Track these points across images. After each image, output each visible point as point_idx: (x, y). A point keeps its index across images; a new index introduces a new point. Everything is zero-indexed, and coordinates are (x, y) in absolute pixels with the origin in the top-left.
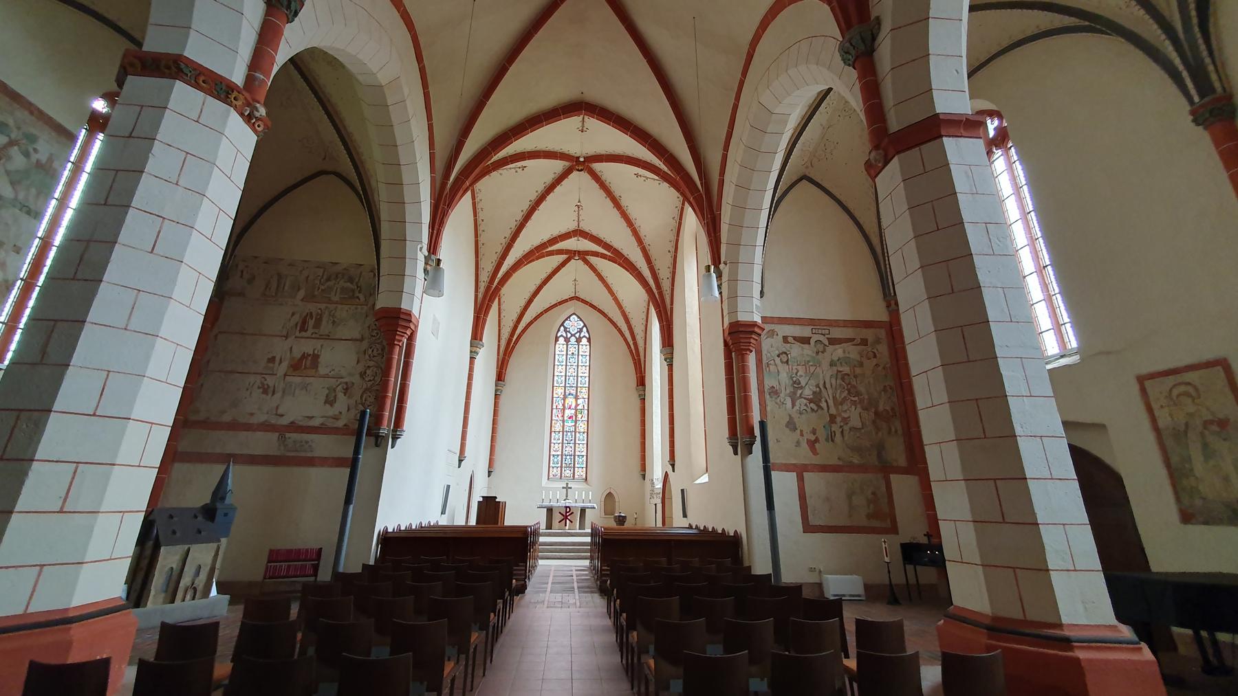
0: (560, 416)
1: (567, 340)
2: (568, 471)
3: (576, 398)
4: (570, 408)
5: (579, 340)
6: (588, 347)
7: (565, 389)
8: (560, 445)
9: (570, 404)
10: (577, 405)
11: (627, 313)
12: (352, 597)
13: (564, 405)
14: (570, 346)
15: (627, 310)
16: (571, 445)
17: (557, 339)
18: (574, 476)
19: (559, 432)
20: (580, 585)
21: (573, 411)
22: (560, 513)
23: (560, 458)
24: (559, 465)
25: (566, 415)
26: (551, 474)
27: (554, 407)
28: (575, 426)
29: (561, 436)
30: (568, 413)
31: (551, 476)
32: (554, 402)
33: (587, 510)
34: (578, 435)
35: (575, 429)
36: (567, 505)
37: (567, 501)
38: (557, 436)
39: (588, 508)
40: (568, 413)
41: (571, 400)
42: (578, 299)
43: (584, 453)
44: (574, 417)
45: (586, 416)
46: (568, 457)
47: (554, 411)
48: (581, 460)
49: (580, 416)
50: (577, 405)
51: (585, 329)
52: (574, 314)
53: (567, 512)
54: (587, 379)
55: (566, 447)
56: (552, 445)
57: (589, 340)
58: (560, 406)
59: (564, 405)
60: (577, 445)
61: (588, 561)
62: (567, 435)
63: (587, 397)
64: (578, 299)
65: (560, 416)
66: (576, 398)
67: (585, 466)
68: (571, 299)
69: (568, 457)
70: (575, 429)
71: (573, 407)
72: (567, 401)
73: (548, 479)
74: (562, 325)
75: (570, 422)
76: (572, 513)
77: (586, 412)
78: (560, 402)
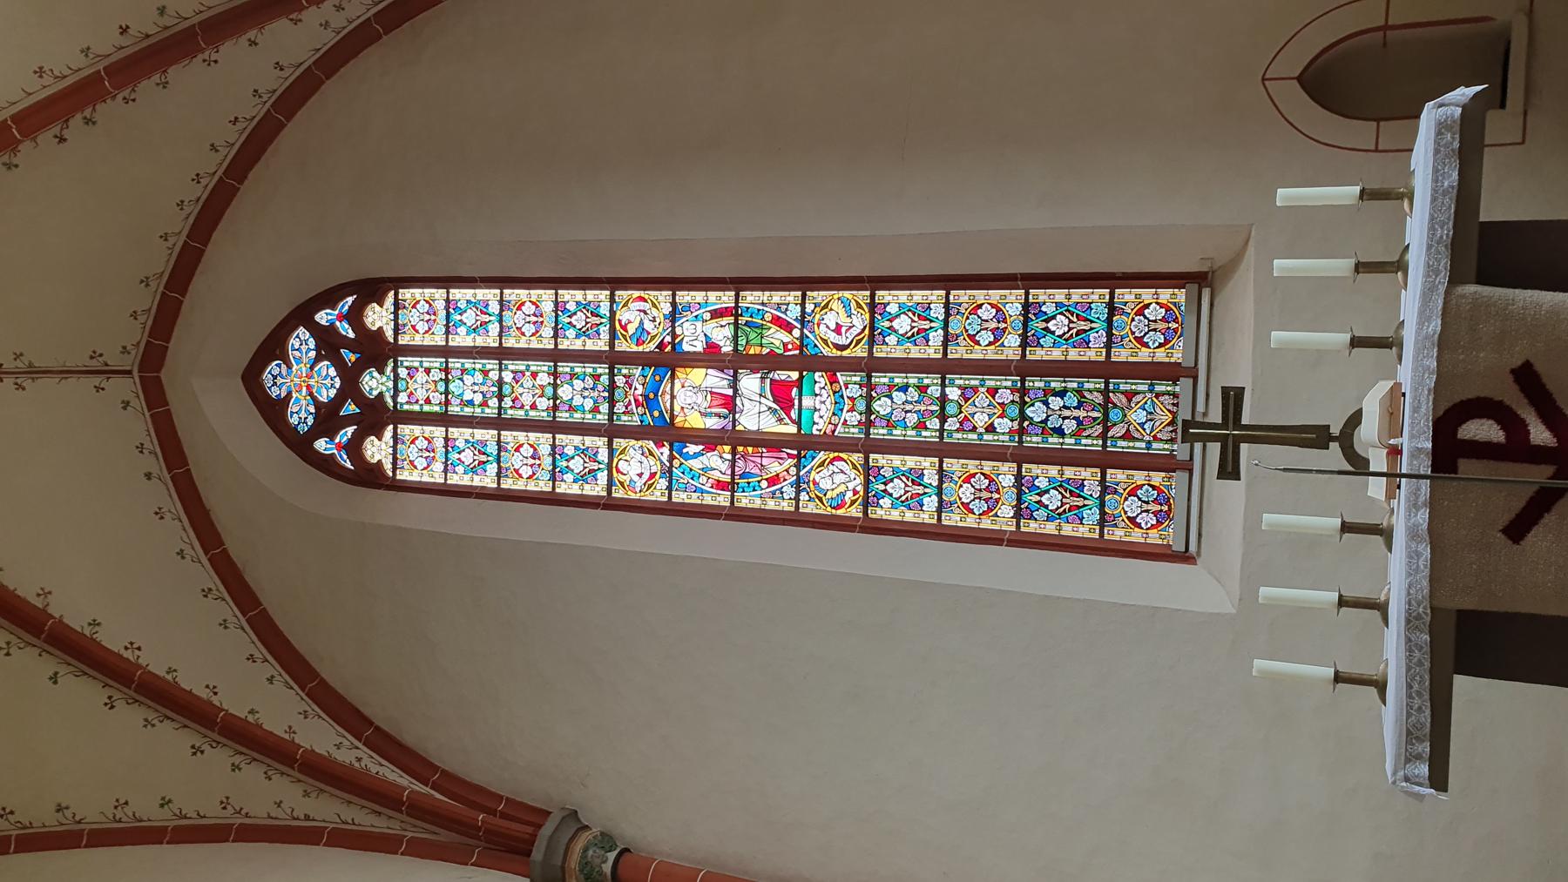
0: (775, 468)
1: (376, 417)
2: (1137, 416)
3: (669, 360)
4: (730, 403)
5: (377, 350)
6: (407, 294)
7: (484, 423)
8: (952, 465)
9: (703, 401)
10: (711, 356)
11: (131, 45)
12: (1275, 275)
13: (709, 441)
14: (403, 398)
15: (108, 44)
16: (953, 393)
17: (371, 477)
18: (1170, 372)
19: (868, 472)
20: (1231, 425)
21: (750, 383)
22: (1517, 530)
23: (1043, 475)
24: (1089, 475)
25: (770, 425)
26: (1154, 538)
27: (723, 499)
28: (833, 368)
29: (896, 460)
30: (756, 415)
31: (1170, 535)
32: (694, 499)
33: (1493, 209)
34: (891, 348)
35: (852, 365)
36: (1416, 440)
37: (1369, 431)
38: (897, 488)
39: (1466, 196)
40: (756, 415)
41: (683, 397)
42: (153, 359)
43: (1013, 302)
44: (781, 375)
45: (777, 297)
46: (1036, 412)
47: (745, 500)
48: (1059, 325)
49: (777, 339)
50: (711, 356)
51: (323, 317)
52: (252, 378)
53: (1517, 449)
54: (571, 296)
55: (966, 424)
56: (952, 519)
57: (371, 290)
58: (717, 463)
59: (709, 441)
60: (957, 352)
61: (1196, 444)
62: (1044, 429)
63: (663, 297)
64: (153, 359)
65: (775, 468)
66: (669, 360)
67: (1098, 296)
68: (154, 395)
69: (1036, 412)
70: (852, 365)
71: (716, 380)
72: (695, 421)
73: (1185, 557)
74: (300, 444)
75: (807, 402)
76: (1526, 377)
77: (751, 298)
78: (696, 464)
